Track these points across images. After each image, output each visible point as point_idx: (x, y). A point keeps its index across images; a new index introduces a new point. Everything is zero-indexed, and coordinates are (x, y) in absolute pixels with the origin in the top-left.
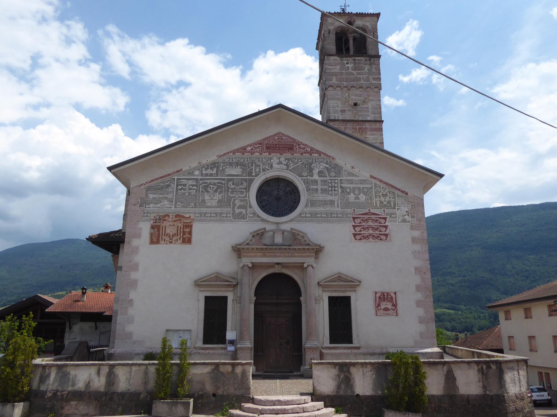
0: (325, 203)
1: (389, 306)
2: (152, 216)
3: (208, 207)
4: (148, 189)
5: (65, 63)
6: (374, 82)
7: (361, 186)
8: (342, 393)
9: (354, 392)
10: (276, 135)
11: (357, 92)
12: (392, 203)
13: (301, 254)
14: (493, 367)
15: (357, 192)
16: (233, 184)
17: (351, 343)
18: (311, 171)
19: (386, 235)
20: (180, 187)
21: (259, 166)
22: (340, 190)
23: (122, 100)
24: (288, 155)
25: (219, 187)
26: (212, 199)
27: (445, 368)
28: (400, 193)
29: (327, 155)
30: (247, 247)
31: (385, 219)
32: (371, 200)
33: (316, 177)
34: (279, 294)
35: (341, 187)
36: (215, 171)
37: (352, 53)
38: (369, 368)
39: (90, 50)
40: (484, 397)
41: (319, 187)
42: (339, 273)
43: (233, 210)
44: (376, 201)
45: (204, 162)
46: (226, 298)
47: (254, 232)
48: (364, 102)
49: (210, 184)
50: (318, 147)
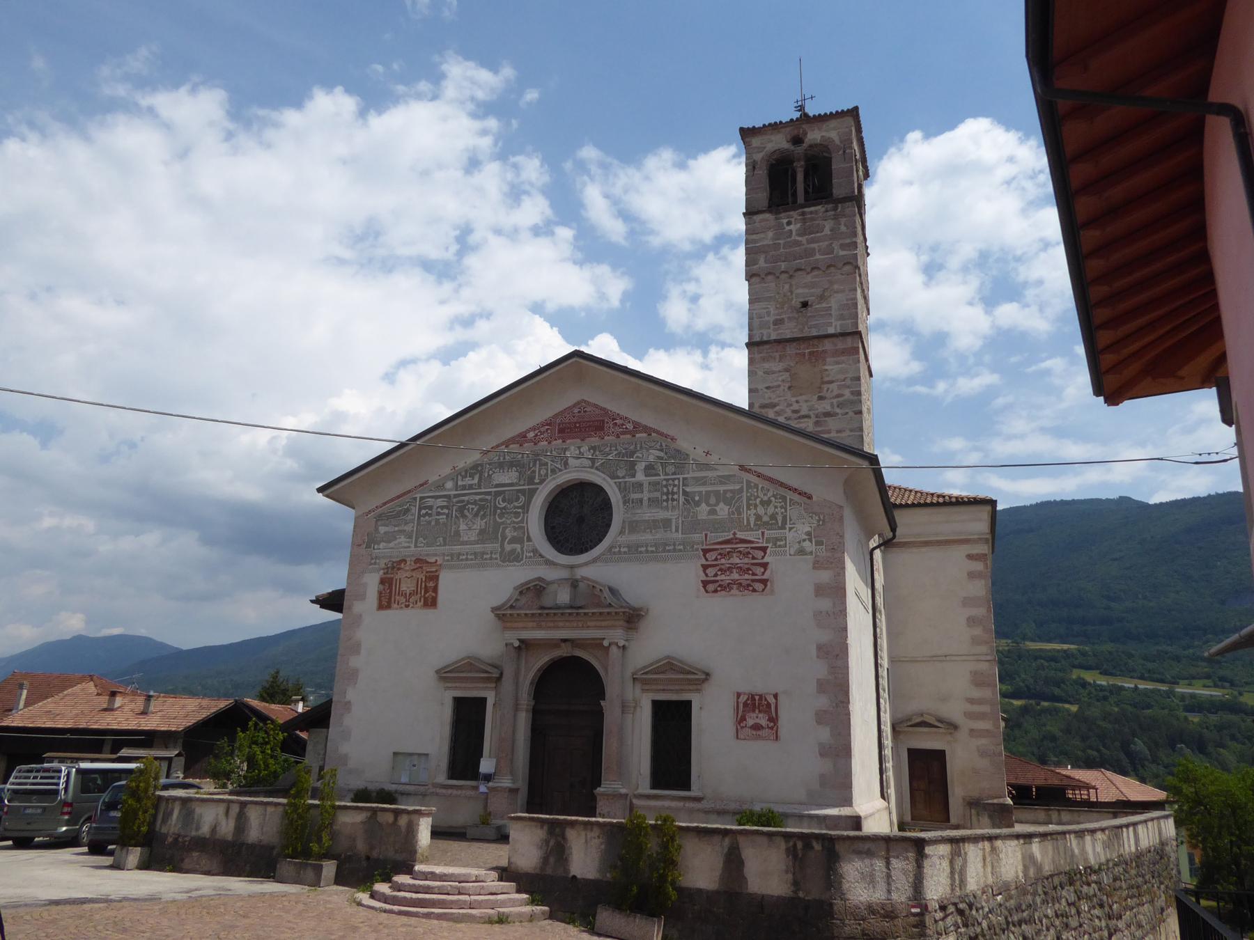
0: (654, 525)
1: (763, 721)
2: (382, 563)
3: (465, 543)
4: (379, 518)
5: (512, 235)
6: (842, 253)
7: (722, 488)
8: (549, 871)
9: (567, 871)
10: (574, 406)
11: (809, 278)
12: (780, 518)
13: (598, 624)
14: (817, 846)
15: (713, 500)
16: (504, 501)
17: (689, 789)
18: (632, 467)
19: (764, 582)
20: (423, 512)
21: (546, 464)
22: (682, 499)
23: (616, 287)
24: (594, 441)
25: (482, 508)
26: (470, 529)
27: (727, 841)
28: (796, 497)
29: (661, 434)
30: (509, 612)
31: (764, 549)
32: (739, 513)
33: (640, 476)
34: (568, 693)
35: (685, 493)
36: (476, 481)
37: (801, 198)
38: (596, 832)
39: (554, 205)
40: (791, 903)
41: (646, 496)
42: (668, 657)
43: (502, 546)
44: (749, 515)
45: (461, 465)
46: (485, 699)
47: (523, 585)
48: (822, 298)
49: (468, 503)
50: (648, 420)
